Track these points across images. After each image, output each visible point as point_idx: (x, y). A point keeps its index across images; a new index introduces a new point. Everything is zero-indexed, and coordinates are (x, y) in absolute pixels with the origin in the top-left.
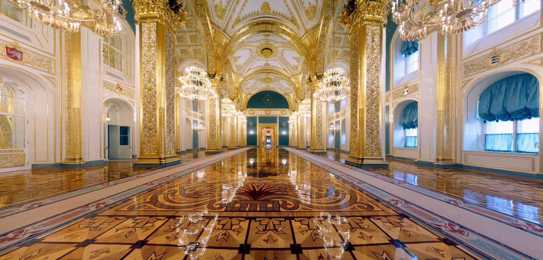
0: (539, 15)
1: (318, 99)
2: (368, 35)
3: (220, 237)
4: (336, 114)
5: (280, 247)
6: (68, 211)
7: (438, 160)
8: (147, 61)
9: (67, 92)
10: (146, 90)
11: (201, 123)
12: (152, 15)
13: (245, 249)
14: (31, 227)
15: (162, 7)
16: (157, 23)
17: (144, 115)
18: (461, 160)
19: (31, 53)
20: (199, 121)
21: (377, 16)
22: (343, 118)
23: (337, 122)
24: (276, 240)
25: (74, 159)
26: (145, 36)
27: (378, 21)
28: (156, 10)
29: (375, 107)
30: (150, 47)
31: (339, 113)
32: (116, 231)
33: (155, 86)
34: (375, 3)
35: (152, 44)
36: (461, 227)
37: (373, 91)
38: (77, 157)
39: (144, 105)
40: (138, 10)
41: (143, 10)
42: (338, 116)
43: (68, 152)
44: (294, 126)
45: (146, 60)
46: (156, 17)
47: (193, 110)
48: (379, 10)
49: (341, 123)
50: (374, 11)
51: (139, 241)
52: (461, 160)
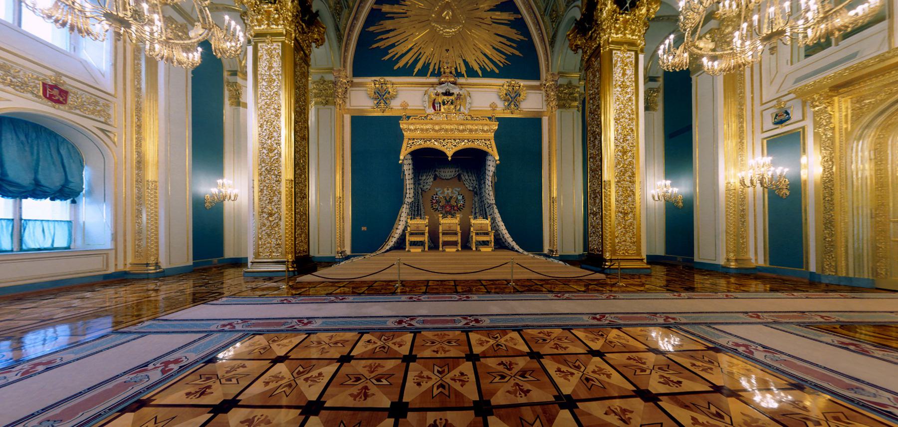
2: (615, 65)
3: (436, 392)
5: (535, 401)
7: (728, 260)
8: (266, 103)
9: (135, 156)
10: (264, 151)
12: (274, 31)
13: (483, 408)
14: (10, 380)
15: (290, 19)
16: (283, 42)
17: (261, 191)
19: (80, 92)
21: (630, 36)
24: (528, 391)
25: (147, 265)
26: (263, 65)
27: (632, 44)
28: (281, 22)
29: (630, 177)
30: (271, 81)
32: (681, 382)
34: (628, 17)
35: (274, 77)
36: (308, 318)
37: (624, 153)
38: (152, 260)
39: (261, 174)
40: (252, 22)
41: (260, 23)
43: (137, 254)
45: (263, 103)
46: (281, 34)
48: (633, 27)
50: (625, 29)
51: (648, 390)
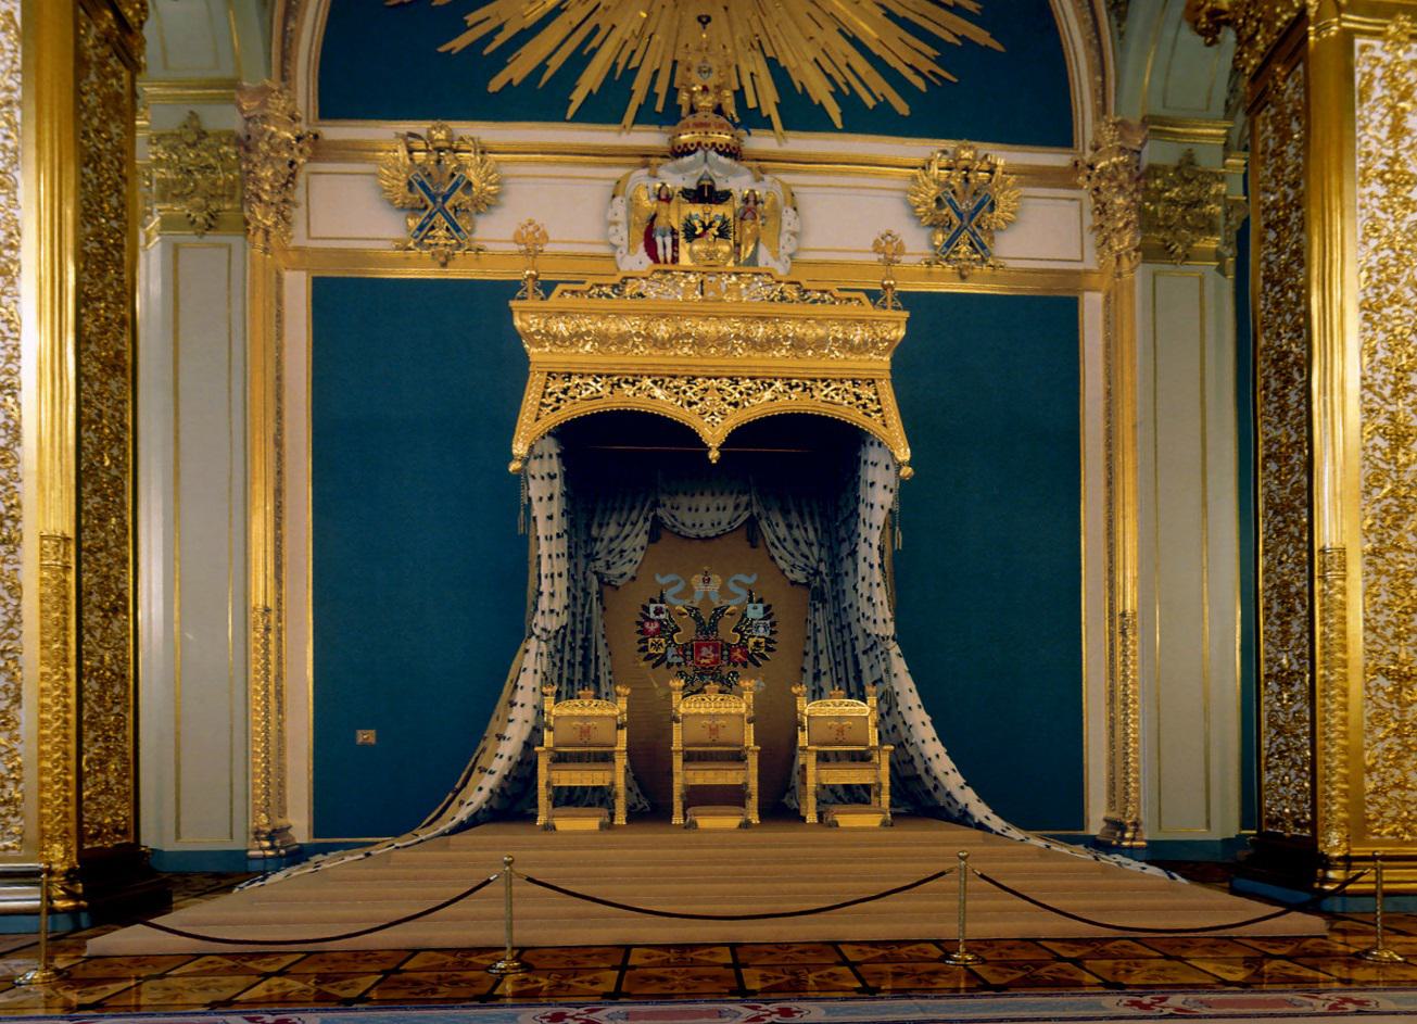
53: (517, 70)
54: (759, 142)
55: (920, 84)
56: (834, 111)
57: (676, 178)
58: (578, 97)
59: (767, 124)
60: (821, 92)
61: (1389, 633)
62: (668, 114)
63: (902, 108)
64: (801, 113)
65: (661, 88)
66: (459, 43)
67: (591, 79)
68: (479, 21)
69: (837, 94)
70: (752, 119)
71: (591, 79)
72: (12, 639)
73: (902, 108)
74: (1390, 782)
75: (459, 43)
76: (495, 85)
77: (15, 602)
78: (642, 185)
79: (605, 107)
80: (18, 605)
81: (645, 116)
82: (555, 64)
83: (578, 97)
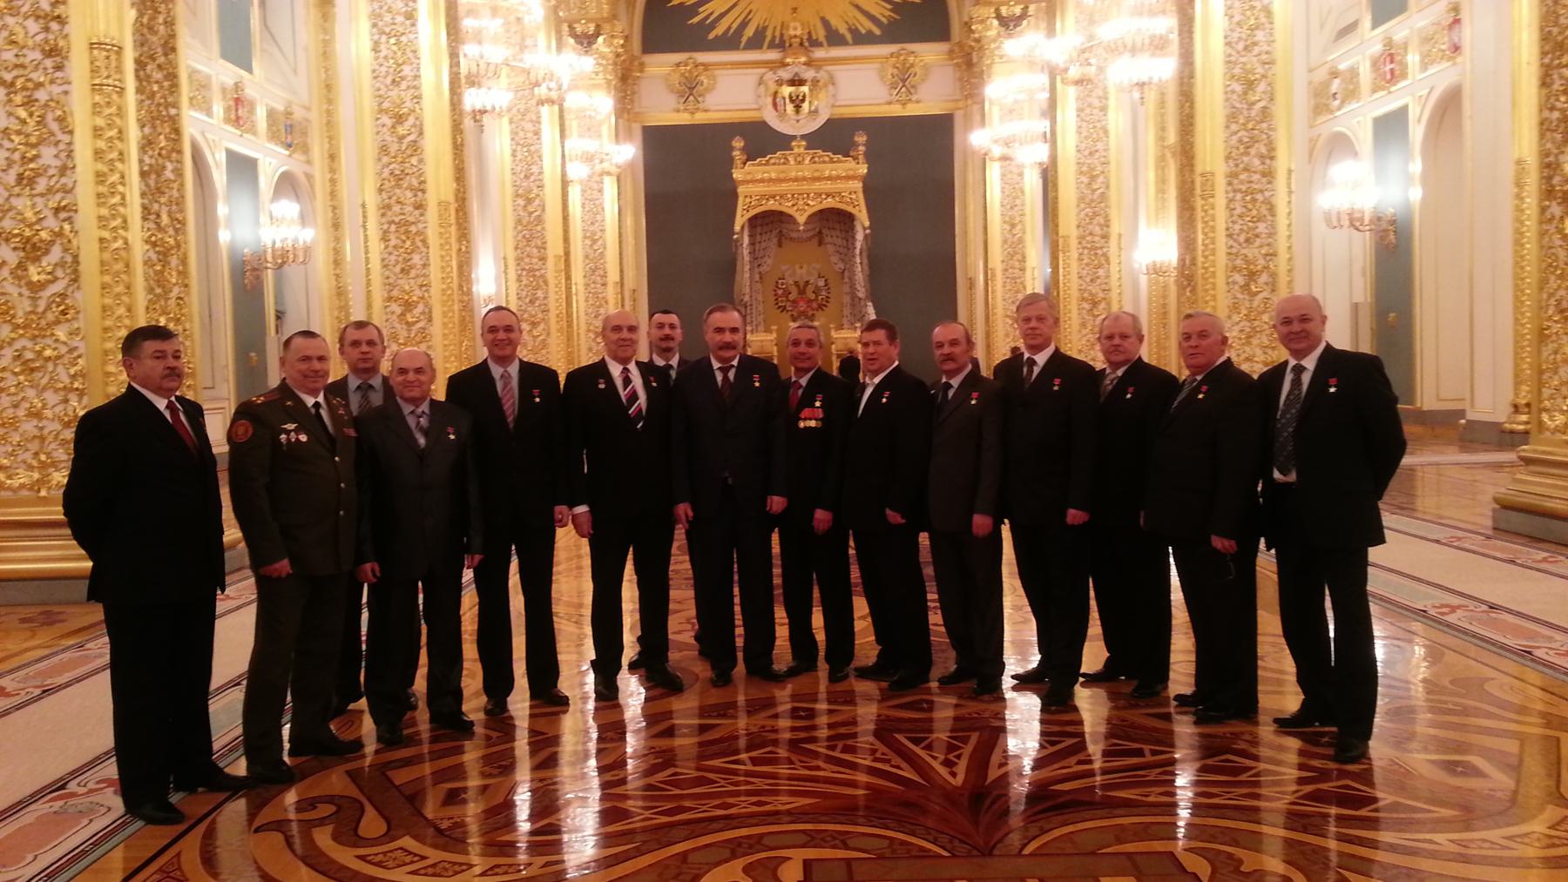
0: (111, 769)
1: (1004, 158)
4: (1370, 41)
6: (78, 680)
11: (287, 184)
18: (369, 306)
20: (271, 161)
22: (1442, 76)
23: (1391, 127)
29: (1262, 157)
31: (1400, 29)
33: (418, 98)
42: (1390, 68)
44: (1013, 193)
47: (225, 55)
49: (1417, 132)
52: (369, 306)
53: (719, 30)
54: (819, 53)
55: (885, 20)
56: (849, 37)
57: (785, 74)
58: (744, 39)
59: (821, 45)
60: (843, 30)
61: (1242, 238)
62: (781, 44)
63: (877, 32)
64: (835, 39)
65: (777, 34)
66: (696, 20)
67: (749, 32)
68: (704, 10)
69: (850, 30)
70: (815, 43)
71: (749, 32)
72: (66, 192)
73: (877, 32)
74: (1244, 356)
75: (696, 20)
76: (711, 36)
77: (66, 138)
78: (770, 77)
79: (756, 43)
80: (70, 144)
81: (772, 46)
82: (735, 26)
83: (744, 39)
